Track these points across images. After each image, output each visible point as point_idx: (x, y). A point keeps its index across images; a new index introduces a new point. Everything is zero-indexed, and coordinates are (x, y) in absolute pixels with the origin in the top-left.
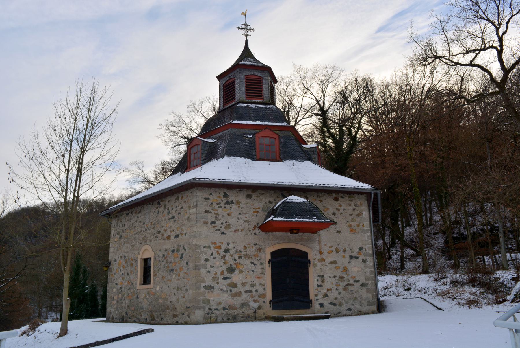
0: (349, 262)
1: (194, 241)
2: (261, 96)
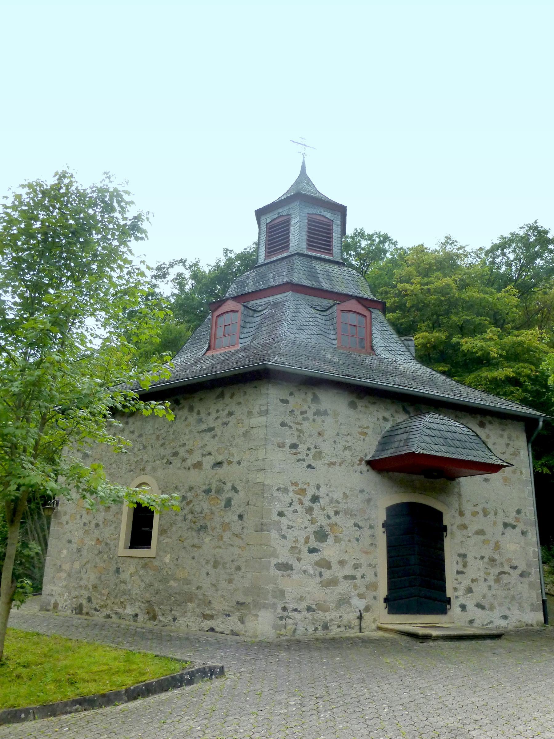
0: (503, 534)
1: (260, 477)
2: (330, 250)
